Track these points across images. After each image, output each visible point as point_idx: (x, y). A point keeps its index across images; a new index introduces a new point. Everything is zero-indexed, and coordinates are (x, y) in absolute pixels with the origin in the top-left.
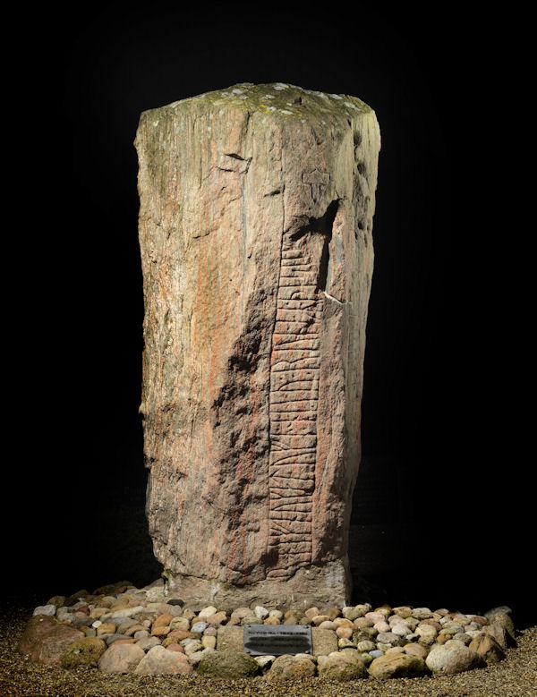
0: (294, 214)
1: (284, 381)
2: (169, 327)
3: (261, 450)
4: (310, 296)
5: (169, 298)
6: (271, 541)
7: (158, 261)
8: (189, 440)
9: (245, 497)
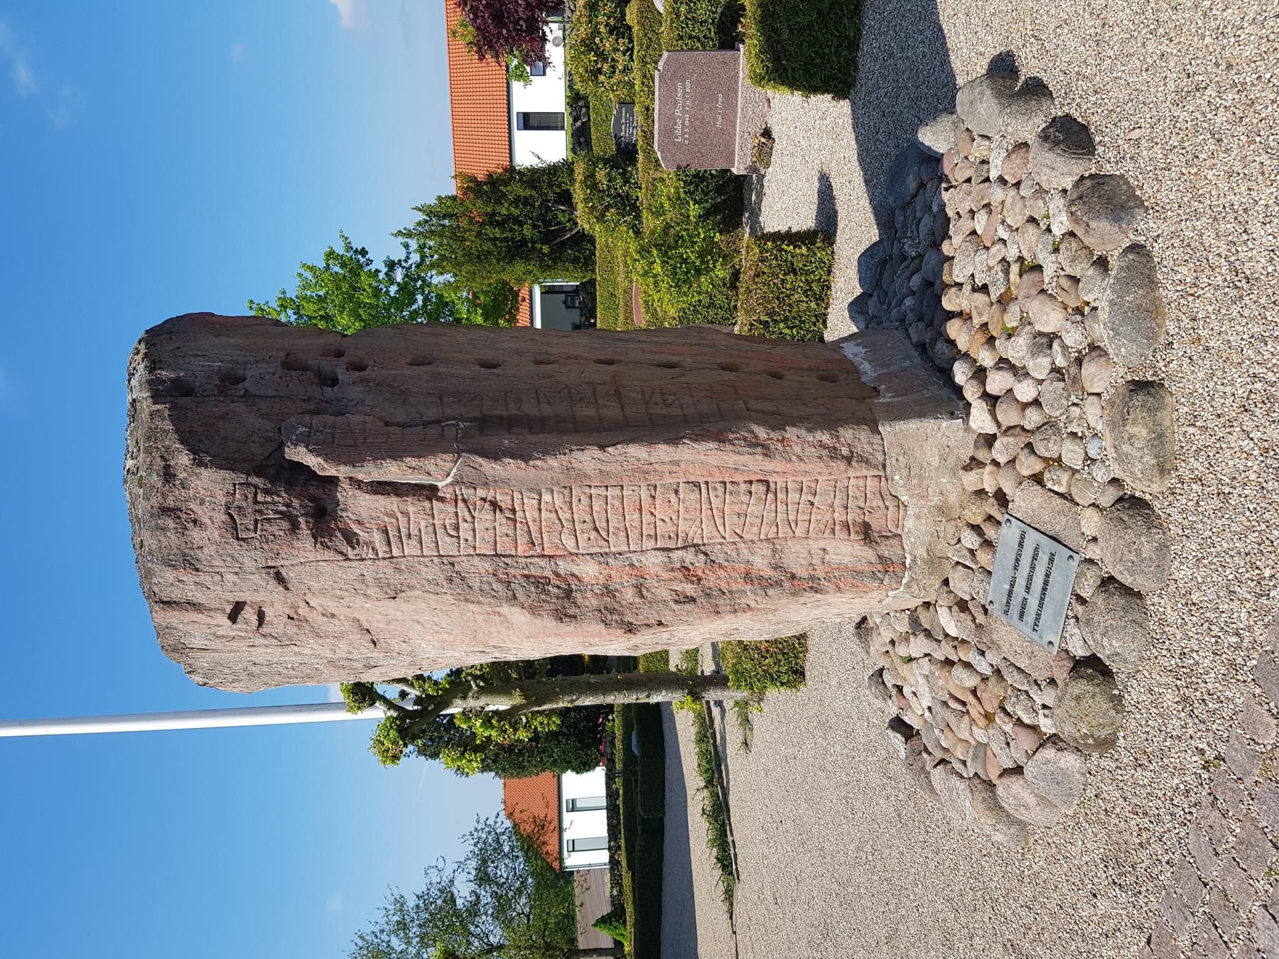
1: (593, 535)
3: (702, 557)
4: (451, 509)
6: (844, 535)
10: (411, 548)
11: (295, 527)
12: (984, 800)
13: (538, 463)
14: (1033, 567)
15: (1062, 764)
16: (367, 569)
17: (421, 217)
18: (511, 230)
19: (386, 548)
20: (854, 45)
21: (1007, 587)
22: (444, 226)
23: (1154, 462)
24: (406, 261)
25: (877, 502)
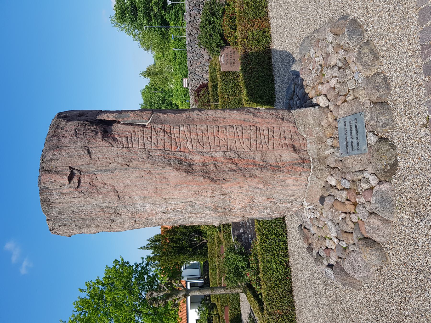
0: (101, 141)
1: (198, 144)
2: (171, 211)
3: (237, 155)
4: (149, 131)
5: (155, 212)
6: (286, 148)
7: (134, 219)
8: (233, 196)
9: (263, 163)
10: (135, 145)
11: (97, 133)
12: (363, 245)
13: (179, 115)
14: (351, 129)
15: (383, 189)
16: (119, 151)
17: (149, 242)
18: (179, 243)
19: (126, 144)
20: (273, 89)
22: (156, 244)
23: (373, 56)
24: (142, 264)
25: (295, 137)
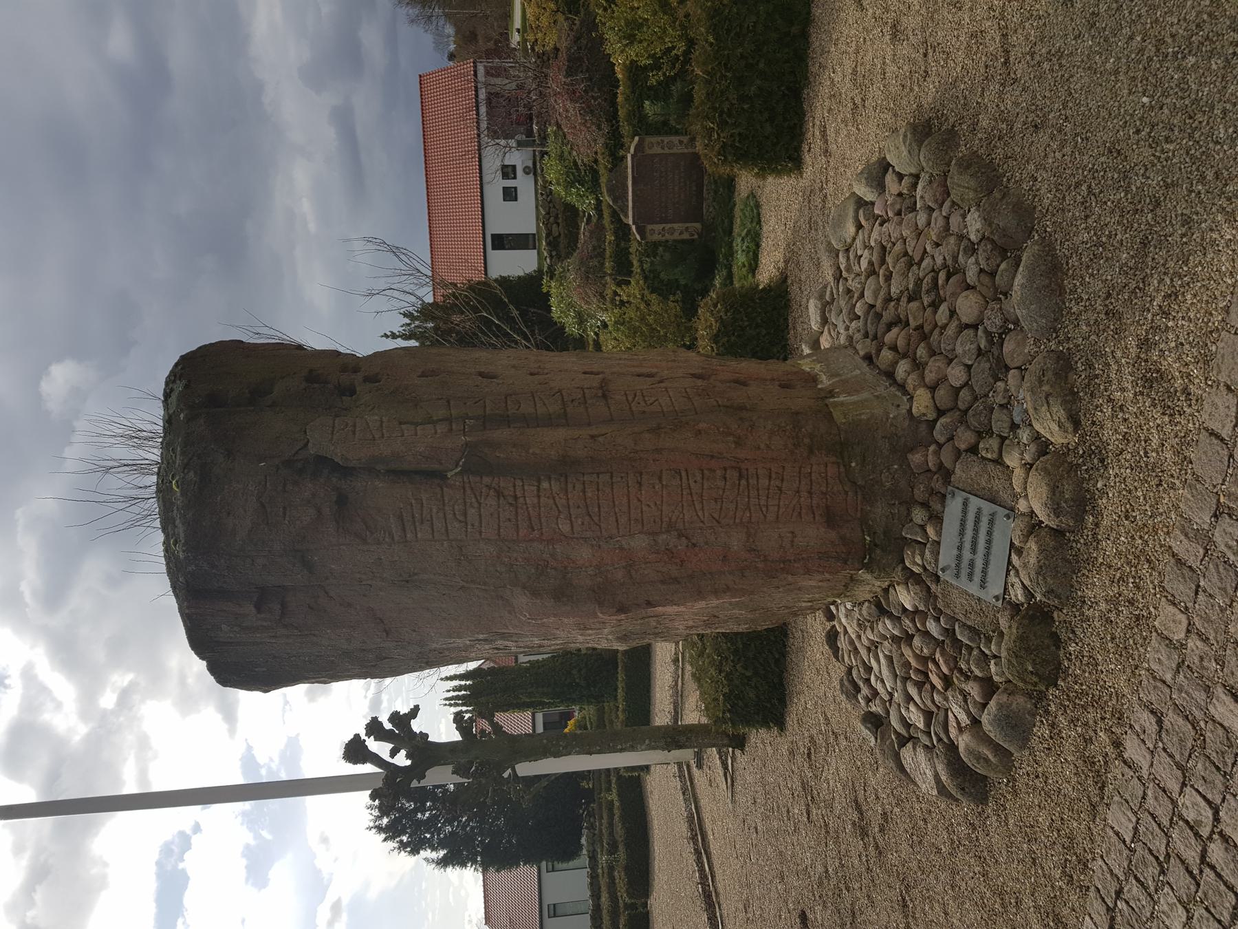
14: (976, 530)
21: (955, 552)
